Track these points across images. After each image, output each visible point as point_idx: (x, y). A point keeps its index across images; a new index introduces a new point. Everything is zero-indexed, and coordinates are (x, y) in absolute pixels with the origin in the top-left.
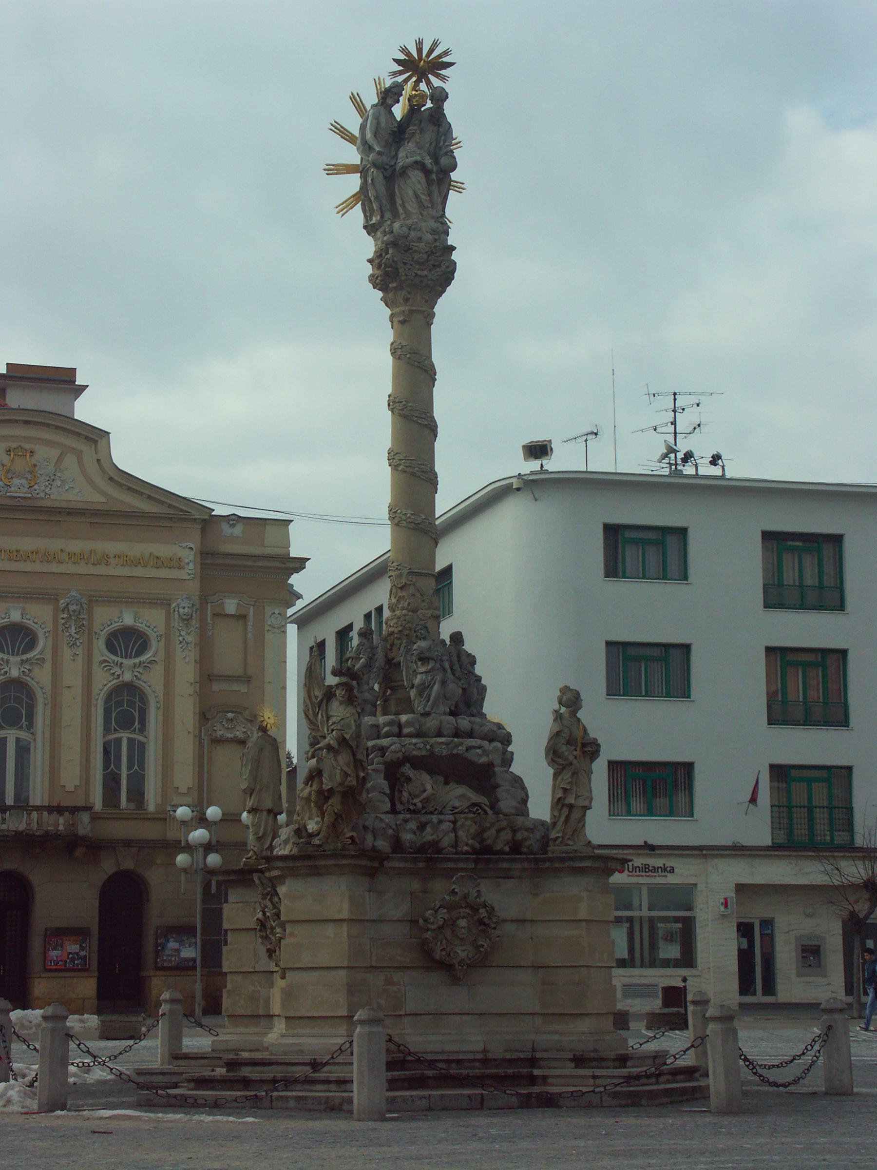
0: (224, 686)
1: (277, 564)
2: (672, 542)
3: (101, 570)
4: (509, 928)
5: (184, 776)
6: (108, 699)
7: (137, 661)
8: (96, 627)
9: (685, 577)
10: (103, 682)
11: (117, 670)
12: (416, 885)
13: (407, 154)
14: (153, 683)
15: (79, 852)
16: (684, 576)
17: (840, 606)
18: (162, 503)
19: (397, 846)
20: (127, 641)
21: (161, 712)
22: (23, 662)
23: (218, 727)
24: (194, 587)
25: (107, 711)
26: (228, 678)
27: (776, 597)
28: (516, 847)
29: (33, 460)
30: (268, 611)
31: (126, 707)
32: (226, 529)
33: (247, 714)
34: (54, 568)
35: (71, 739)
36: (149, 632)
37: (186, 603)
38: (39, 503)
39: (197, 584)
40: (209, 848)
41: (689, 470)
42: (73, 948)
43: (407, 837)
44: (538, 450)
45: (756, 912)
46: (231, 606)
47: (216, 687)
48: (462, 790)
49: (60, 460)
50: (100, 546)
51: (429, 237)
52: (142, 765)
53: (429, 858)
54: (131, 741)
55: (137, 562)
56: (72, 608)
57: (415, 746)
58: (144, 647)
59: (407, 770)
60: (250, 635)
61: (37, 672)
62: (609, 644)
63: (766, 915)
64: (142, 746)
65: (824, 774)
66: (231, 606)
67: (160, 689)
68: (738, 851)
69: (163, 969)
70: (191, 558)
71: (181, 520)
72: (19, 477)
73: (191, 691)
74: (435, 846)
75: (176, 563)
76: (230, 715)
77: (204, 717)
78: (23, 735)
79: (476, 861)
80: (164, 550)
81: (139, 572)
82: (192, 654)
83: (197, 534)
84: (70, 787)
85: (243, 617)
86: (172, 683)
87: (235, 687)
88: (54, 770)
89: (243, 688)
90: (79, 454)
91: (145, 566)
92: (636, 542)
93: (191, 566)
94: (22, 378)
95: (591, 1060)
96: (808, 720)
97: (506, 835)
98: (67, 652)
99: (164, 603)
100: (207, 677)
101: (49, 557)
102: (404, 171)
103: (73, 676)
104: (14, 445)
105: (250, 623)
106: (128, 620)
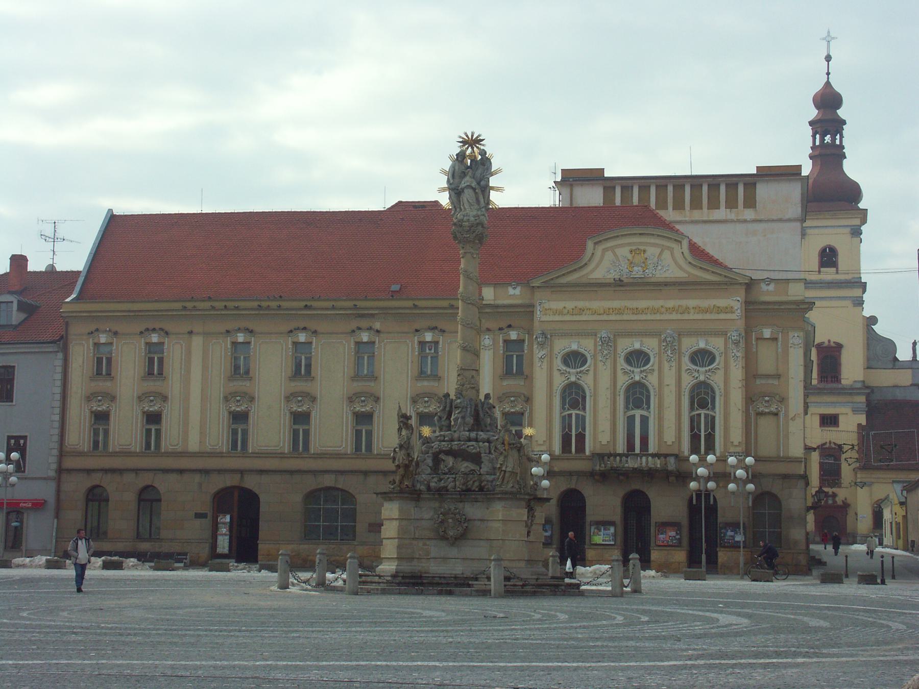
0: (763, 381)
1: (794, 307)
3: (686, 317)
4: (478, 523)
5: (737, 436)
7: (707, 368)
8: (684, 349)
10: (559, 382)
12: (437, 505)
13: (467, 181)
14: (717, 381)
15: (672, 479)
18: (720, 275)
19: (429, 488)
20: (702, 357)
21: (722, 398)
22: (641, 372)
24: (741, 324)
25: (563, 399)
26: (768, 376)
28: (481, 489)
29: (646, 256)
30: (791, 334)
31: (702, 396)
32: (764, 287)
34: (658, 317)
35: (670, 415)
36: (714, 351)
37: (735, 334)
38: (649, 280)
39: (743, 321)
40: (708, 479)
42: (673, 533)
43: (432, 484)
46: (767, 333)
47: (758, 382)
48: (466, 464)
49: (660, 254)
50: (684, 303)
51: (472, 219)
52: (713, 428)
53: (441, 493)
54: (706, 416)
55: (706, 311)
56: (668, 339)
57: (445, 445)
58: (713, 360)
59: (442, 456)
60: (780, 350)
61: (584, 377)
66: (767, 333)
67: (722, 386)
69: (725, 547)
70: (739, 306)
72: (638, 266)
73: (740, 385)
74: (445, 488)
75: (729, 310)
76: (767, 398)
77: (750, 399)
78: (645, 413)
79: (461, 495)
80: (722, 303)
81: (707, 316)
82: (741, 363)
83: (743, 292)
85: (775, 339)
86: (728, 382)
87: (770, 381)
88: (202, 433)
89: (776, 382)
90: (671, 250)
91: (711, 313)
93: (739, 311)
94: (767, 175)
97: (477, 484)
98: (666, 365)
99: (724, 334)
100: (751, 374)
101: (655, 311)
102: (463, 190)
103: (670, 378)
104: (634, 248)
105: (779, 343)
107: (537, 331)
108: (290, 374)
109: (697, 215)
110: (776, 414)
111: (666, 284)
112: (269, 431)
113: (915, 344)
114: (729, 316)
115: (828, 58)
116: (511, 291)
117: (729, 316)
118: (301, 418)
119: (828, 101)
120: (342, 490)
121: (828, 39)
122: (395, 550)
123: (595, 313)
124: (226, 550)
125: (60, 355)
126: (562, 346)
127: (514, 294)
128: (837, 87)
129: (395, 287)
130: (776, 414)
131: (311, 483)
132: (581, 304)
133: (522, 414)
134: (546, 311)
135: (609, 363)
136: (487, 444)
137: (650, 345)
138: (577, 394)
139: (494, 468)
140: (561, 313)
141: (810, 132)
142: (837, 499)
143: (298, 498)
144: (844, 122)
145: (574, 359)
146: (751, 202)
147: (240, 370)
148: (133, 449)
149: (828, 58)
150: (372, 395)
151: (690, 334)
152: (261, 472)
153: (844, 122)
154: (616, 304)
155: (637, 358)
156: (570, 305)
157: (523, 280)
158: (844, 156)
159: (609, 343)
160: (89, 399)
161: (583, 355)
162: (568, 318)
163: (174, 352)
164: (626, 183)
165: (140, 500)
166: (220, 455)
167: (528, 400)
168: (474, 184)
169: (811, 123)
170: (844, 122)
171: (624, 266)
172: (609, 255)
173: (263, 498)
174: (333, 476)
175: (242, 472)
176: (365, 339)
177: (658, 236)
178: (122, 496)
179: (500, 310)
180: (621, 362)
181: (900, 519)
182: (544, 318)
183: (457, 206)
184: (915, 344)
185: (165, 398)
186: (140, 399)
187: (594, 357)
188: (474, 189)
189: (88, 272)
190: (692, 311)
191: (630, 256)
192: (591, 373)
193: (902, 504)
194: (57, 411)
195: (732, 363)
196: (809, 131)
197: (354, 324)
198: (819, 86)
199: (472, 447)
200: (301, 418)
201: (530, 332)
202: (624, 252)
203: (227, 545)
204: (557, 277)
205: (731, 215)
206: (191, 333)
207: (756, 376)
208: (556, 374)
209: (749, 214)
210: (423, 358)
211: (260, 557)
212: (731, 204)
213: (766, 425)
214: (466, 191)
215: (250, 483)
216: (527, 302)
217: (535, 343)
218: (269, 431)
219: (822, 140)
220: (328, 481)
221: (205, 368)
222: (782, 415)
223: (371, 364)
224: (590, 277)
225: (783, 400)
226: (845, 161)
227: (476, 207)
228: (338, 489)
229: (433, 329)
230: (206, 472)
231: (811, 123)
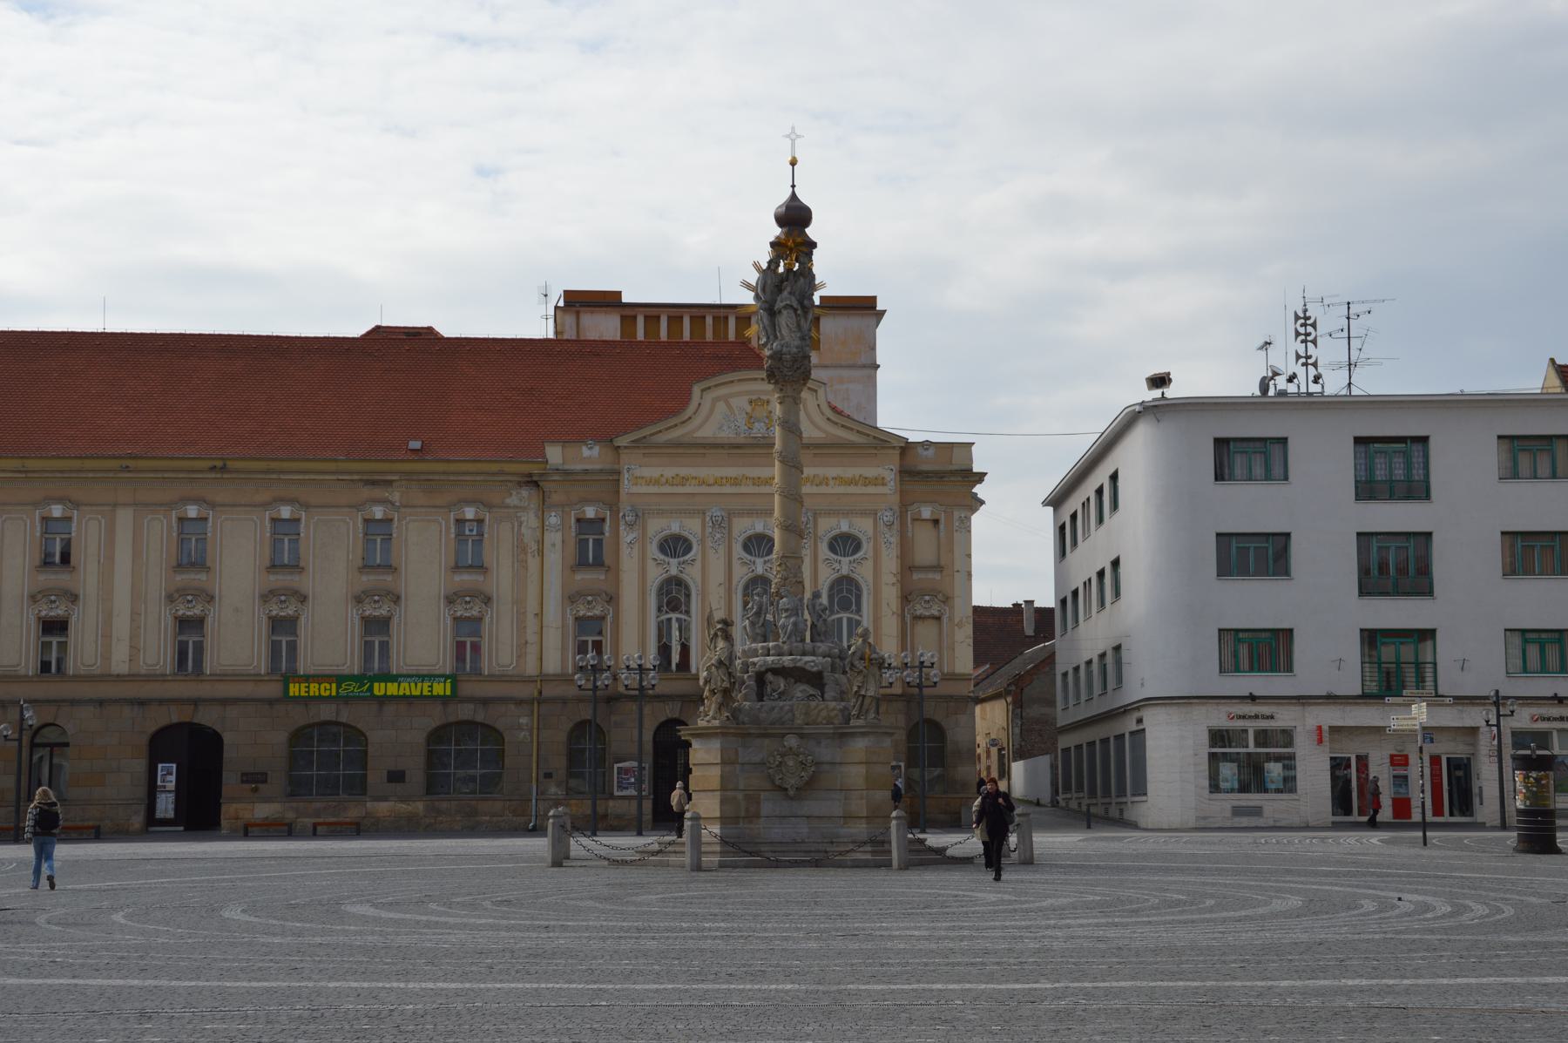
0: (922, 576)
2: (1276, 450)
8: (821, 532)
9: (1286, 478)
10: (655, 576)
11: (836, 566)
14: (864, 574)
17: (1428, 497)
27: (1367, 490)
31: (674, 595)
33: (940, 596)
36: (860, 536)
41: (1292, 388)
44: (1160, 381)
45: (1350, 750)
47: (916, 576)
54: (849, 620)
55: (852, 482)
58: (689, 549)
59: (770, 677)
61: (688, 569)
62: (1218, 535)
63: (1362, 752)
65: (1557, 635)
66: (926, 513)
67: (699, 580)
68: (1331, 699)
75: (768, 481)
77: (906, 598)
80: (871, 472)
83: (897, 458)
85: (936, 522)
87: (931, 576)
88: (134, 648)
89: (937, 577)
95: (1051, 866)
96: (1398, 591)
100: (907, 567)
106: (845, 527)
107: (625, 507)
108: (37, 562)
110: (938, 618)
112: (236, 644)
115: (793, 163)
116: (586, 452)
118: (282, 626)
120: (483, 725)
121: (793, 137)
122: (717, 807)
123: (703, 483)
124: (171, 814)
126: (659, 527)
127: (591, 455)
129: (415, 444)
130: (938, 618)
131: (300, 717)
132: (684, 471)
134: (637, 480)
135: (722, 550)
138: (679, 592)
139: (842, 692)
140: (656, 482)
143: (280, 737)
144: (814, 245)
145: (675, 546)
147: (191, 557)
148: (22, 672)
149: (793, 163)
150: (389, 592)
151: (830, 513)
152: (225, 702)
153: (814, 245)
154: (732, 472)
156: (669, 472)
157: (605, 438)
159: (723, 524)
161: (686, 540)
163: (87, 534)
164: (652, 312)
166: (160, 678)
167: (612, 599)
168: (795, 304)
171: (741, 421)
172: (721, 406)
173: (227, 738)
174: (472, 706)
175: (196, 702)
178: (631, 738)
180: (738, 550)
182: (635, 490)
185: (74, 598)
186: (33, 598)
187: (702, 541)
190: (831, 482)
192: (698, 564)
197: (367, 492)
199: (810, 662)
200: (282, 626)
201: (614, 507)
202: (741, 403)
203: (171, 806)
206: (115, 505)
208: (650, 564)
210: (276, 544)
211: (224, 823)
213: (925, 632)
214: (785, 312)
216: (608, 466)
217: (622, 523)
218: (236, 644)
221: (136, 554)
222: (945, 619)
223: (386, 551)
224: (699, 434)
228: (337, 724)
229: (60, 500)
230: (142, 703)
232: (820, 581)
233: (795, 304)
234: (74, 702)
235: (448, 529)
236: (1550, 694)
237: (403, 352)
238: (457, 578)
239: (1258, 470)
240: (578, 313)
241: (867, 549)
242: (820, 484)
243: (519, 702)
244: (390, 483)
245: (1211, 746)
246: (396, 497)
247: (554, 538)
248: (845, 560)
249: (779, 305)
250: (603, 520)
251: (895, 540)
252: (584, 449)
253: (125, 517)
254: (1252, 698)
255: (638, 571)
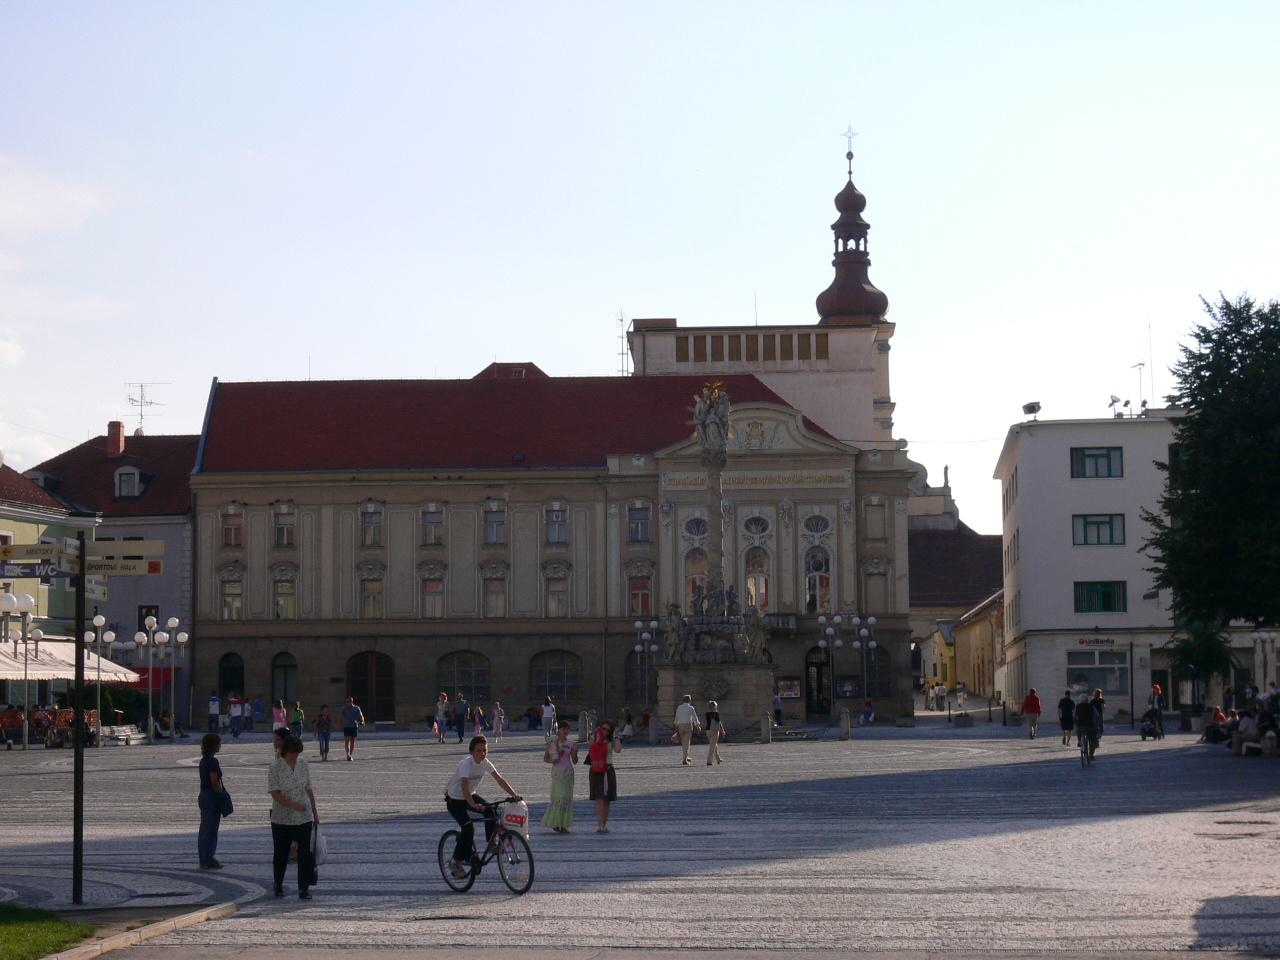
2: (1117, 522)
6: (747, 555)
10: (804, 546)
14: (831, 545)
16: (1125, 610)
23: (869, 567)
34: (775, 486)
41: (1126, 412)
44: (1032, 408)
46: (875, 500)
49: (776, 428)
54: (821, 577)
57: (705, 629)
58: (826, 525)
59: (703, 636)
64: (827, 579)
66: (875, 500)
71: (843, 455)
77: (860, 561)
80: (834, 472)
82: (852, 529)
84: (788, 603)
89: (883, 545)
92: (1090, 456)
98: (784, 532)
100: (861, 538)
103: (787, 543)
107: (662, 500)
109: (770, 364)
110: (884, 575)
111: (782, 456)
113: (946, 469)
114: (840, 485)
115: (850, 156)
116: (635, 462)
117: (840, 485)
119: (850, 202)
120: (568, 652)
121: (850, 135)
125: (189, 527)
127: (638, 464)
128: (860, 188)
130: (884, 575)
133: (649, 578)
136: (737, 626)
137: (768, 513)
141: (833, 238)
142: (682, 611)
146: (823, 352)
149: (850, 156)
152: (396, 637)
155: (758, 523)
158: (868, 263)
160: (219, 569)
162: (691, 488)
165: (275, 666)
167: (655, 564)
168: (717, 421)
169: (833, 227)
170: (868, 226)
175: (375, 637)
176: (495, 508)
177: (774, 410)
179: (627, 480)
181: (946, 661)
182: (669, 488)
183: (704, 437)
184: (946, 469)
186: (271, 568)
188: (717, 424)
189: (206, 437)
191: (748, 430)
193: (949, 645)
194: (188, 581)
195: (844, 528)
196: (831, 234)
198: (841, 187)
204: (680, 450)
205: (804, 365)
207: (866, 540)
209: (821, 364)
212: (804, 354)
214: (711, 426)
215: (383, 647)
219: (845, 245)
220: (462, 644)
222: (889, 575)
225: (890, 562)
226: (870, 269)
227: (719, 438)
230: (342, 638)
231: (833, 227)
232: (800, 550)
233: (717, 421)
234: (299, 638)
235: (542, 517)
236: (1093, 627)
237: (512, 387)
238: (548, 551)
239: (1103, 469)
240: (644, 336)
241: (832, 525)
242: (798, 482)
243: (591, 635)
244: (501, 486)
245: (1069, 663)
246: (506, 495)
247: (614, 524)
248: (817, 535)
249: (708, 422)
250: (648, 509)
251: (851, 520)
252: (634, 460)
253: (327, 513)
254: (1097, 630)
255: (672, 542)
